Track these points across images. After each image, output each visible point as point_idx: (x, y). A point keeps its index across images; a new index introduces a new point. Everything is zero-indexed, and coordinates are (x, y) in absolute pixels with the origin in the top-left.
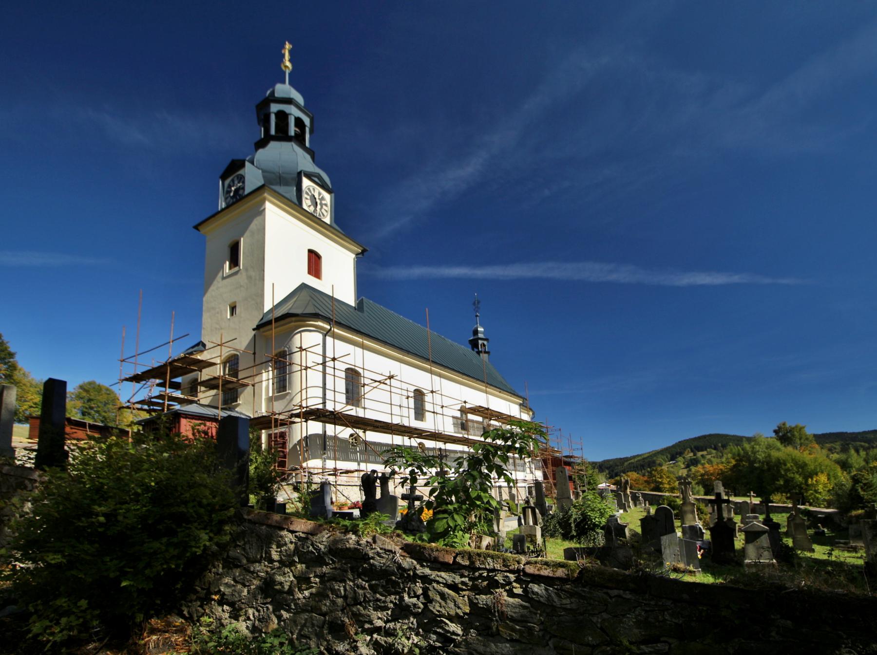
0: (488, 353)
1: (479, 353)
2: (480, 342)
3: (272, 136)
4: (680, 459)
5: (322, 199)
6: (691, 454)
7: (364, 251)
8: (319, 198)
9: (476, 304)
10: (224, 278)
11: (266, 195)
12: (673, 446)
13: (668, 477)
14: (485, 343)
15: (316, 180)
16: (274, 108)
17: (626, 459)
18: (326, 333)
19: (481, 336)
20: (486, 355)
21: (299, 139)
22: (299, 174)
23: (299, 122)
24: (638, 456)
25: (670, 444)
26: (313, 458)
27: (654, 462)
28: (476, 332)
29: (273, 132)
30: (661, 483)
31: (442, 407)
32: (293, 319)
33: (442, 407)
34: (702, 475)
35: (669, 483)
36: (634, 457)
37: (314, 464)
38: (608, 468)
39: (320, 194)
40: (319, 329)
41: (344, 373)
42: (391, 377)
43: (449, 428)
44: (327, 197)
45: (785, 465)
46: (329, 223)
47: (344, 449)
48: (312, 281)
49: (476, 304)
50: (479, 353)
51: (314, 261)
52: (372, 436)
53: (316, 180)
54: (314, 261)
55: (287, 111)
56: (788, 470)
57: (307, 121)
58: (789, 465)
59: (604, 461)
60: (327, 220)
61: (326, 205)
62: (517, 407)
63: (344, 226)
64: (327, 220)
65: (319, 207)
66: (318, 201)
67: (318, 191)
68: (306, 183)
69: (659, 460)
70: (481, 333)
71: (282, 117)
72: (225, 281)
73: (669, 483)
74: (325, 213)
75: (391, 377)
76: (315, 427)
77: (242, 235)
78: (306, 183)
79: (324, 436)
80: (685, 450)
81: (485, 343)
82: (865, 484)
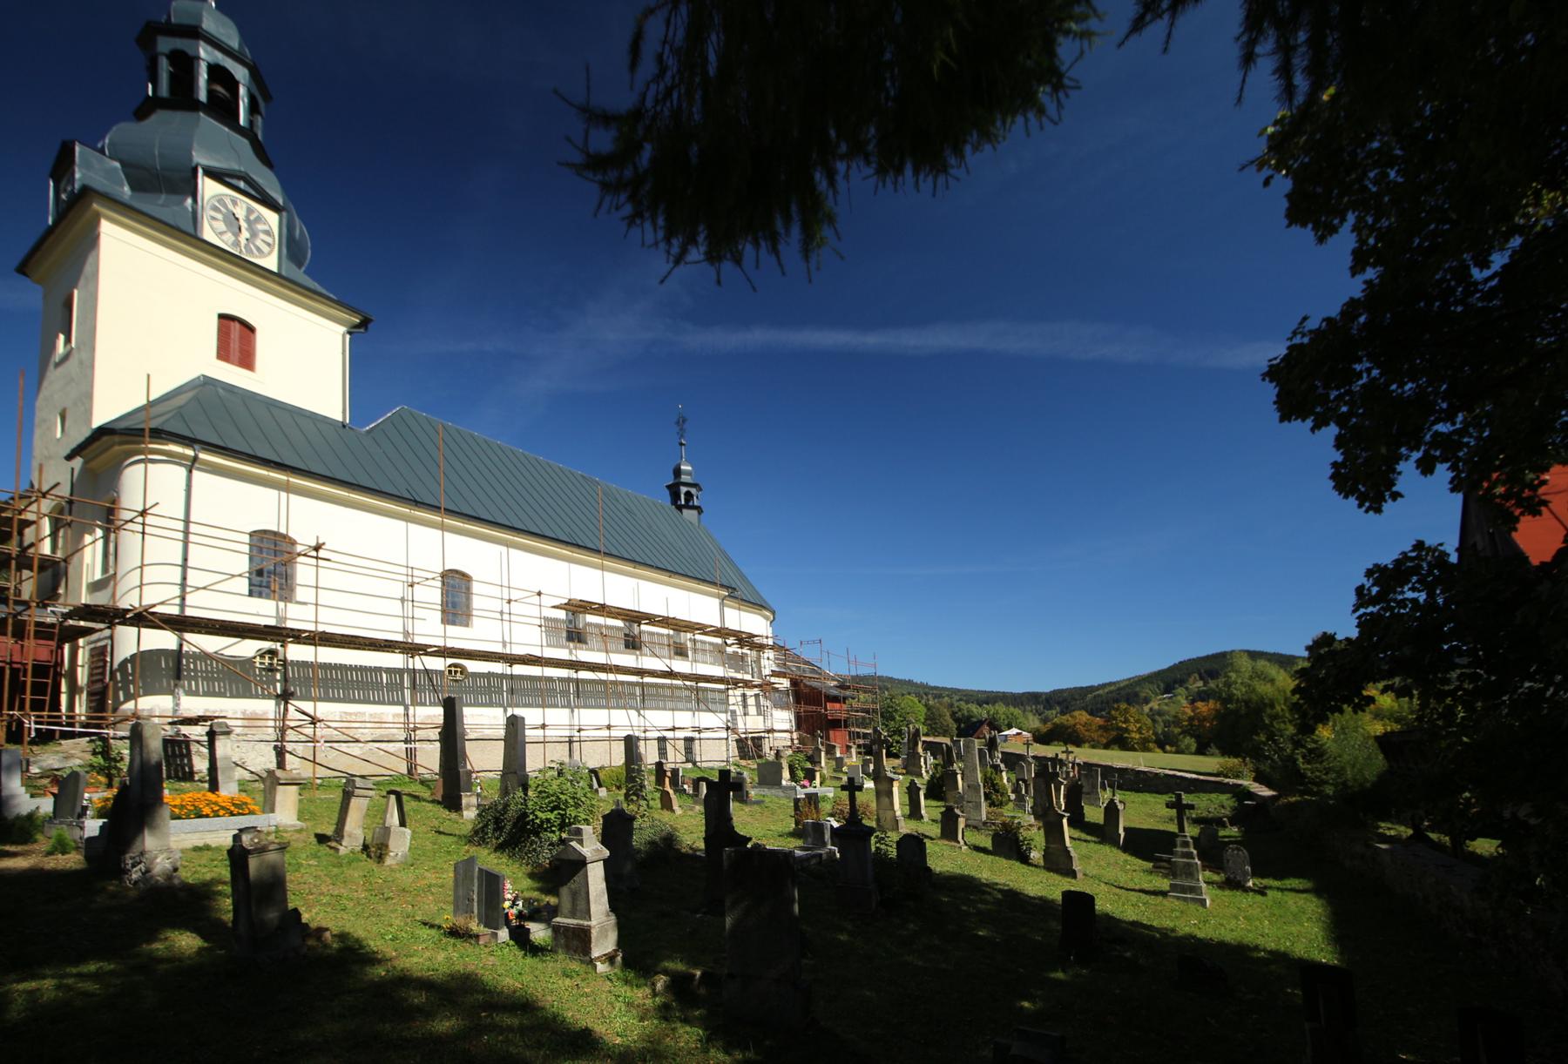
0: (698, 508)
1: (680, 508)
2: (684, 489)
3: (163, 99)
4: (1181, 690)
5: (259, 219)
6: (1200, 684)
7: (365, 323)
8: (263, 231)
9: (681, 422)
10: (57, 365)
11: (95, 206)
12: (1170, 669)
13: (1138, 721)
14: (693, 491)
15: (242, 184)
16: (165, 44)
17: (1091, 689)
18: (192, 465)
19: (684, 478)
20: (695, 512)
21: (223, 109)
22: (195, 171)
23: (217, 72)
24: (1110, 684)
25: (1165, 666)
26: (145, 694)
27: (1136, 695)
28: (677, 472)
29: (164, 91)
30: (1127, 730)
31: (509, 602)
32: (117, 438)
33: (509, 602)
34: (1191, 719)
35: (1139, 731)
36: (1104, 686)
37: (156, 705)
38: (1059, 703)
39: (250, 211)
40: (173, 459)
41: (247, 539)
42: (317, 548)
43: (528, 640)
44: (272, 218)
45: (1272, 706)
46: (275, 269)
47: (235, 677)
48: (230, 374)
49: (681, 422)
50: (680, 508)
51: (236, 338)
52: (473, 666)
53: (242, 184)
54: (236, 338)
55: (191, 52)
56: (1275, 717)
57: (240, 73)
58: (1278, 708)
59: (1054, 692)
60: (271, 262)
61: (268, 233)
62: (715, 603)
63: (313, 271)
64: (271, 262)
65: (245, 234)
66: (244, 225)
67: (243, 206)
68: (209, 189)
69: (1145, 691)
70: (688, 473)
71: (184, 65)
72: (60, 369)
73: (1139, 731)
74: (265, 249)
75: (317, 548)
76: (163, 640)
77: (75, 286)
78: (209, 189)
79: (178, 655)
80: (1189, 675)
81: (693, 491)
82: (1311, 751)
